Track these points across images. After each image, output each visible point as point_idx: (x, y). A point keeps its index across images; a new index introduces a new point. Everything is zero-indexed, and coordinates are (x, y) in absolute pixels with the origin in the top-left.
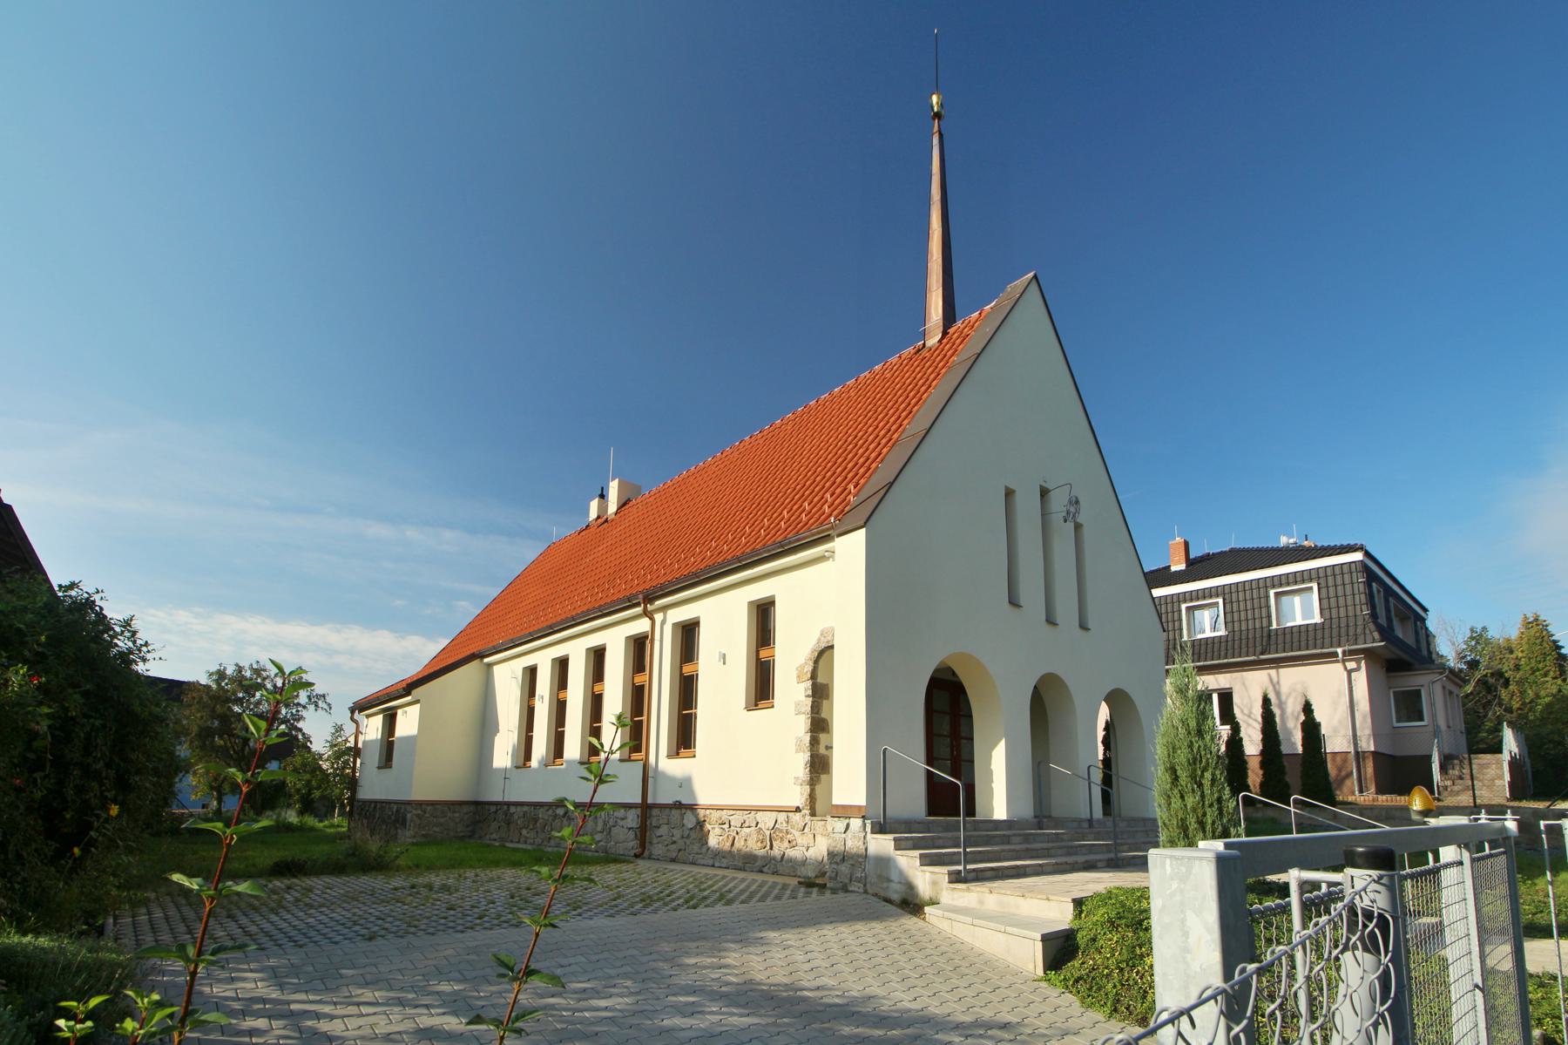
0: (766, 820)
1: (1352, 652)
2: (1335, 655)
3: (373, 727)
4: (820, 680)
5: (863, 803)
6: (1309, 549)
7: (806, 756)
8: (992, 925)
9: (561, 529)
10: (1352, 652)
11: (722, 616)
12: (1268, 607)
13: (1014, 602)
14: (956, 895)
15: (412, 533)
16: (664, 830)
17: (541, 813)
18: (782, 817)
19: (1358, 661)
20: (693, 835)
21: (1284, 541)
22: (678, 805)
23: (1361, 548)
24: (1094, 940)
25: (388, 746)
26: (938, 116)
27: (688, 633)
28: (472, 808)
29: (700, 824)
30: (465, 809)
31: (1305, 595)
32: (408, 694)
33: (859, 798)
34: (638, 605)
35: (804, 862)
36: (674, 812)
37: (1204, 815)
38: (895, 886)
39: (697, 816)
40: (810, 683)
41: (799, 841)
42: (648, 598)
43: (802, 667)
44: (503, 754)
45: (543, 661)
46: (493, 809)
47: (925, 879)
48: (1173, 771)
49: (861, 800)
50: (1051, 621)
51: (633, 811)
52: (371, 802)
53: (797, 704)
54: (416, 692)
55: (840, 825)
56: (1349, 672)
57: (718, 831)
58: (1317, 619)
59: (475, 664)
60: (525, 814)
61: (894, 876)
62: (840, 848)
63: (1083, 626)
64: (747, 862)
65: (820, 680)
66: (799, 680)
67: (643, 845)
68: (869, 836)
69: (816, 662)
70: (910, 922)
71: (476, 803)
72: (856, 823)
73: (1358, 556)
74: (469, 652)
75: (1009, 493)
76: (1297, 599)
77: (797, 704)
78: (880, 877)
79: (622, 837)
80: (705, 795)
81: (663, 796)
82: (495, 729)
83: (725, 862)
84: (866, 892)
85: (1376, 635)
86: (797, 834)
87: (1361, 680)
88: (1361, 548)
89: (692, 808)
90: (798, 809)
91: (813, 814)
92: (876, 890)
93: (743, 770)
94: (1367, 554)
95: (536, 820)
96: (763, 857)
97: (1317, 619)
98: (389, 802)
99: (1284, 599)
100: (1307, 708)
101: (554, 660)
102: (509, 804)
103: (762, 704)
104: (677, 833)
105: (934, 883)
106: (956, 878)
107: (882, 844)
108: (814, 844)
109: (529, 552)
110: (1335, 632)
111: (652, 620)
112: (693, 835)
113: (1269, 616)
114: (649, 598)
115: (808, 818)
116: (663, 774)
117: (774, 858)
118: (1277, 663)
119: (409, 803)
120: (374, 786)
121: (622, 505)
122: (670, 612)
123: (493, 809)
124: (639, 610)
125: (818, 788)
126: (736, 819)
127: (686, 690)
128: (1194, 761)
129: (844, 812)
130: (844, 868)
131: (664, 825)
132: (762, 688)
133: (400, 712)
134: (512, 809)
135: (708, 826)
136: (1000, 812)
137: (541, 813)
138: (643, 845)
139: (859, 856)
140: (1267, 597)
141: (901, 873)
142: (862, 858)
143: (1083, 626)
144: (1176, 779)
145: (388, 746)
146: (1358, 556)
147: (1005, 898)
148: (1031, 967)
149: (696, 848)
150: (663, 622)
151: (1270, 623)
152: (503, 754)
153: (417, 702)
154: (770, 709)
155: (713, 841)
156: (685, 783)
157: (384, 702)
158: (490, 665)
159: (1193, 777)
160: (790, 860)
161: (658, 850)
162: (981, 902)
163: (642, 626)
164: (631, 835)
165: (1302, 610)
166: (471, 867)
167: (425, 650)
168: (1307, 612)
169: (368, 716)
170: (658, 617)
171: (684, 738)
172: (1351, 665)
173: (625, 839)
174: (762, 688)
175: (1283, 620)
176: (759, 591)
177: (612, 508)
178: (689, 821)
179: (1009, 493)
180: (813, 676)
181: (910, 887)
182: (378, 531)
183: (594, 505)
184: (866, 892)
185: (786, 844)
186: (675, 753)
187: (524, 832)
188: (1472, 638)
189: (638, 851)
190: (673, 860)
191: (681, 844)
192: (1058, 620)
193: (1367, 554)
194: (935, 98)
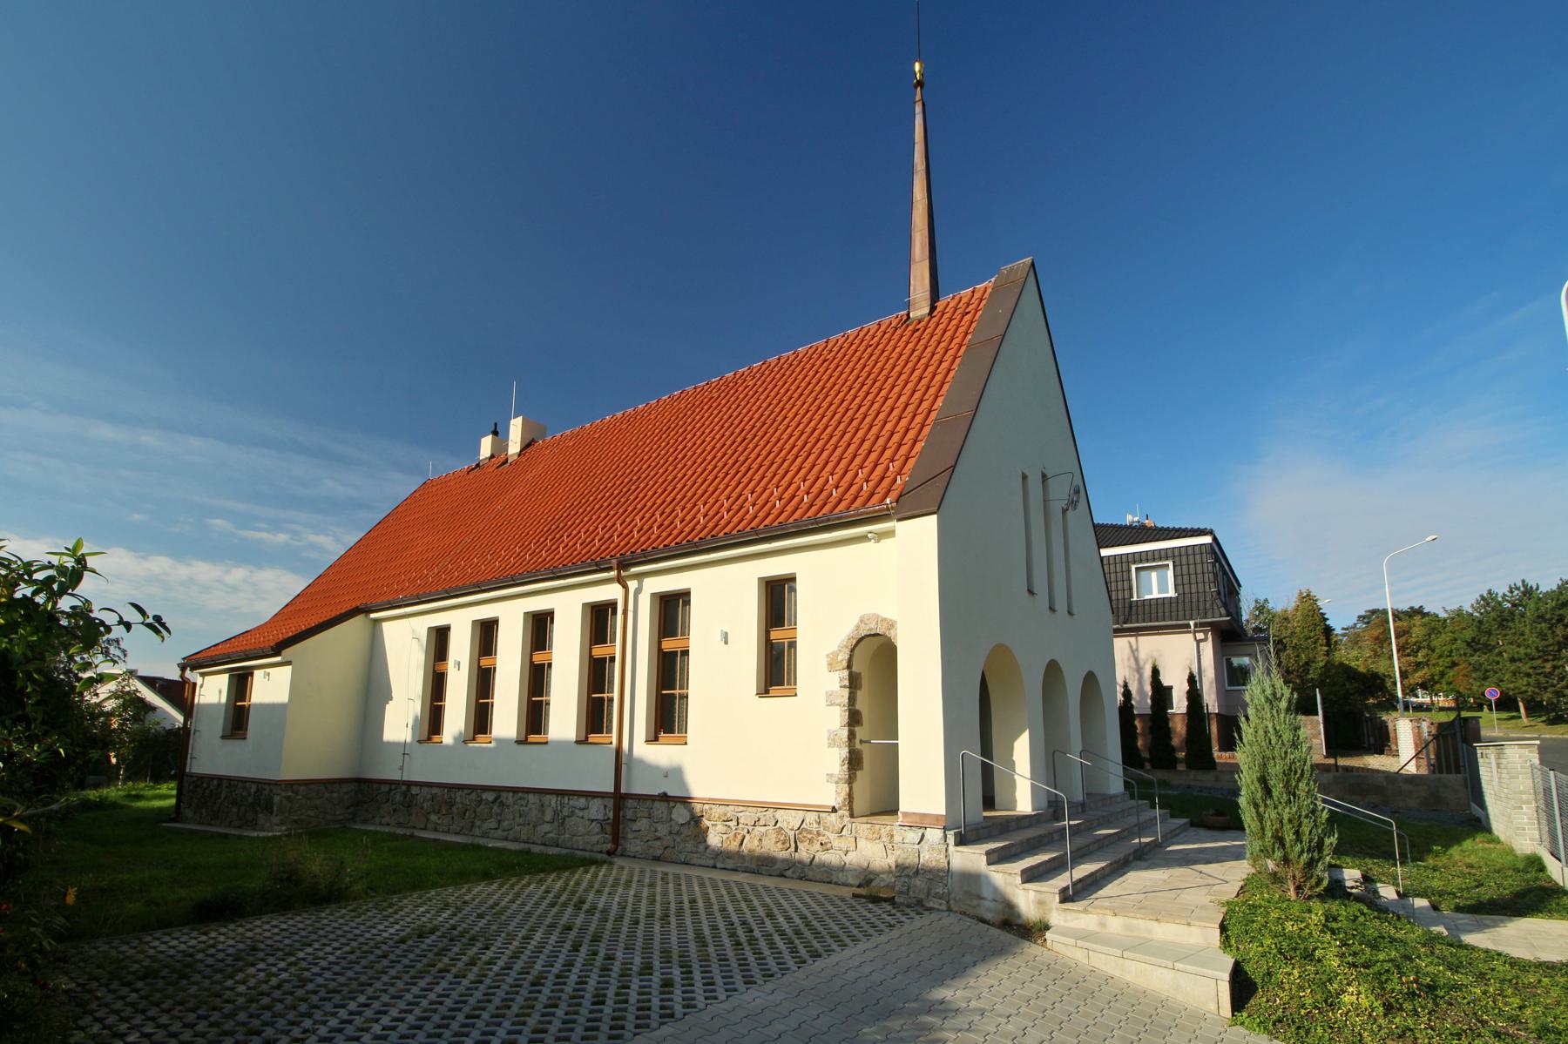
0: (790, 820)
1: (1202, 625)
2: (1188, 626)
3: (212, 689)
4: (854, 669)
5: (943, 812)
6: (1155, 529)
7: (845, 752)
8: (1154, 960)
9: (441, 465)
10: (1202, 625)
11: (722, 595)
12: (1130, 580)
13: (1031, 592)
14: (1070, 916)
15: (148, 439)
16: (642, 824)
17: (459, 796)
18: (811, 817)
19: (1205, 633)
20: (686, 831)
21: (1129, 519)
22: (664, 797)
23: (1210, 532)
24: (1269, 974)
25: (238, 717)
26: (920, 84)
27: (671, 610)
28: (354, 786)
29: (696, 820)
30: (345, 788)
31: (1161, 571)
32: (278, 654)
33: (937, 804)
34: (609, 569)
35: (842, 868)
36: (657, 804)
37: (1300, 825)
38: (991, 905)
39: (691, 811)
40: (846, 673)
41: (836, 844)
42: (624, 563)
43: (835, 654)
44: (400, 722)
45: (461, 621)
46: (385, 788)
47: (1028, 900)
48: (1263, 780)
49: (941, 809)
50: (1052, 609)
51: (596, 804)
52: (211, 778)
53: (830, 695)
54: (288, 653)
55: (913, 836)
56: (1198, 642)
57: (720, 827)
58: (1171, 593)
59: (357, 623)
60: (434, 797)
61: (986, 893)
62: (911, 860)
63: (1070, 613)
64: (763, 865)
65: (854, 669)
66: (831, 667)
67: (616, 840)
68: (952, 848)
69: (852, 650)
70: (1031, 949)
71: (359, 781)
72: (934, 835)
73: (1207, 539)
74: (342, 600)
75: (1024, 477)
76: (1154, 575)
77: (830, 695)
78: (968, 894)
79: (581, 829)
80: (701, 787)
81: (638, 785)
82: (387, 696)
83: (730, 864)
84: (949, 910)
85: (1223, 610)
86: (832, 836)
87: (1208, 649)
88: (1210, 532)
89: (685, 801)
90: (834, 810)
91: (852, 816)
92: (963, 908)
93: (754, 760)
94: (1215, 539)
95: (451, 804)
96: (784, 860)
97: (1171, 593)
98: (243, 781)
99: (1143, 573)
100: (1155, 672)
101: (474, 622)
102: (409, 784)
103: (774, 690)
104: (663, 829)
105: (1040, 903)
106: (1066, 897)
107: (971, 858)
108: (869, 849)
109: (402, 487)
110: (1187, 606)
111: (625, 587)
112: (686, 831)
113: (1131, 589)
114: (624, 565)
115: (847, 819)
116: (641, 762)
117: (800, 862)
118: (1137, 632)
119: (277, 783)
120: (212, 756)
121: (527, 446)
122: (647, 581)
123: (385, 788)
124: (613, 574)
125: (855, 786)
126: (747, 817)
127: (669, 670)
128: (1288, 772)
129: (921, 822)
130: (917, 882)
131: (643, 822)
132: (776, 670)
133: (257, 673)
134: (414, 790)
135: (706, 822)
136: (1024, 804)
137: (459, 796)
138: (616, 840)
139: (941, 870)
140: (1129, 571)
141: (996, 890)
142: (938, 876)
143: (1070, 613)
144: (1268, 792)
145: (238, 717)
146: (1207, 539)
147: (1134, 922)
148: (1213, 1007)
149: (690, 846)
150: (638, 591)
151: (1131, 596)
152: (400, 722)
153: (288, 663)
154: (792, 694)
155: (714, 840)
156: (676, 773)
157: (238, 657)
158: (377, 621)
159: (1287, 785)
160: (822, 865)
161: (634, 846)
162: (1103, 925)
163: (612, 592)
164: (595, 827)
165: (1158, 585)
166: (434, 886)
167: (269, 592)
168: (1163, 587)
169: (203, 675)
170: (633, 585)
171: (667, 717)
172: (1200, 636)
173: (597, 840)
174: (776, 670)
175: (1143, 590)
176: (775, 567)
177: (514, 447)
178: (680, 815)
179: (1024, 477)
180: (849, 666)
181: (1009, 906)
182: (105, 431)
183: (486, 446)
184: (949, 910)
185: (818, 846)
186: (653, 739)
187: (433, 817)
188: (1257, 608)
189: (609, 846)
190: (657, 859)
191: (668, 840)
192: (1075, 611)
193: (1215, 539)
194: (917, 67)
